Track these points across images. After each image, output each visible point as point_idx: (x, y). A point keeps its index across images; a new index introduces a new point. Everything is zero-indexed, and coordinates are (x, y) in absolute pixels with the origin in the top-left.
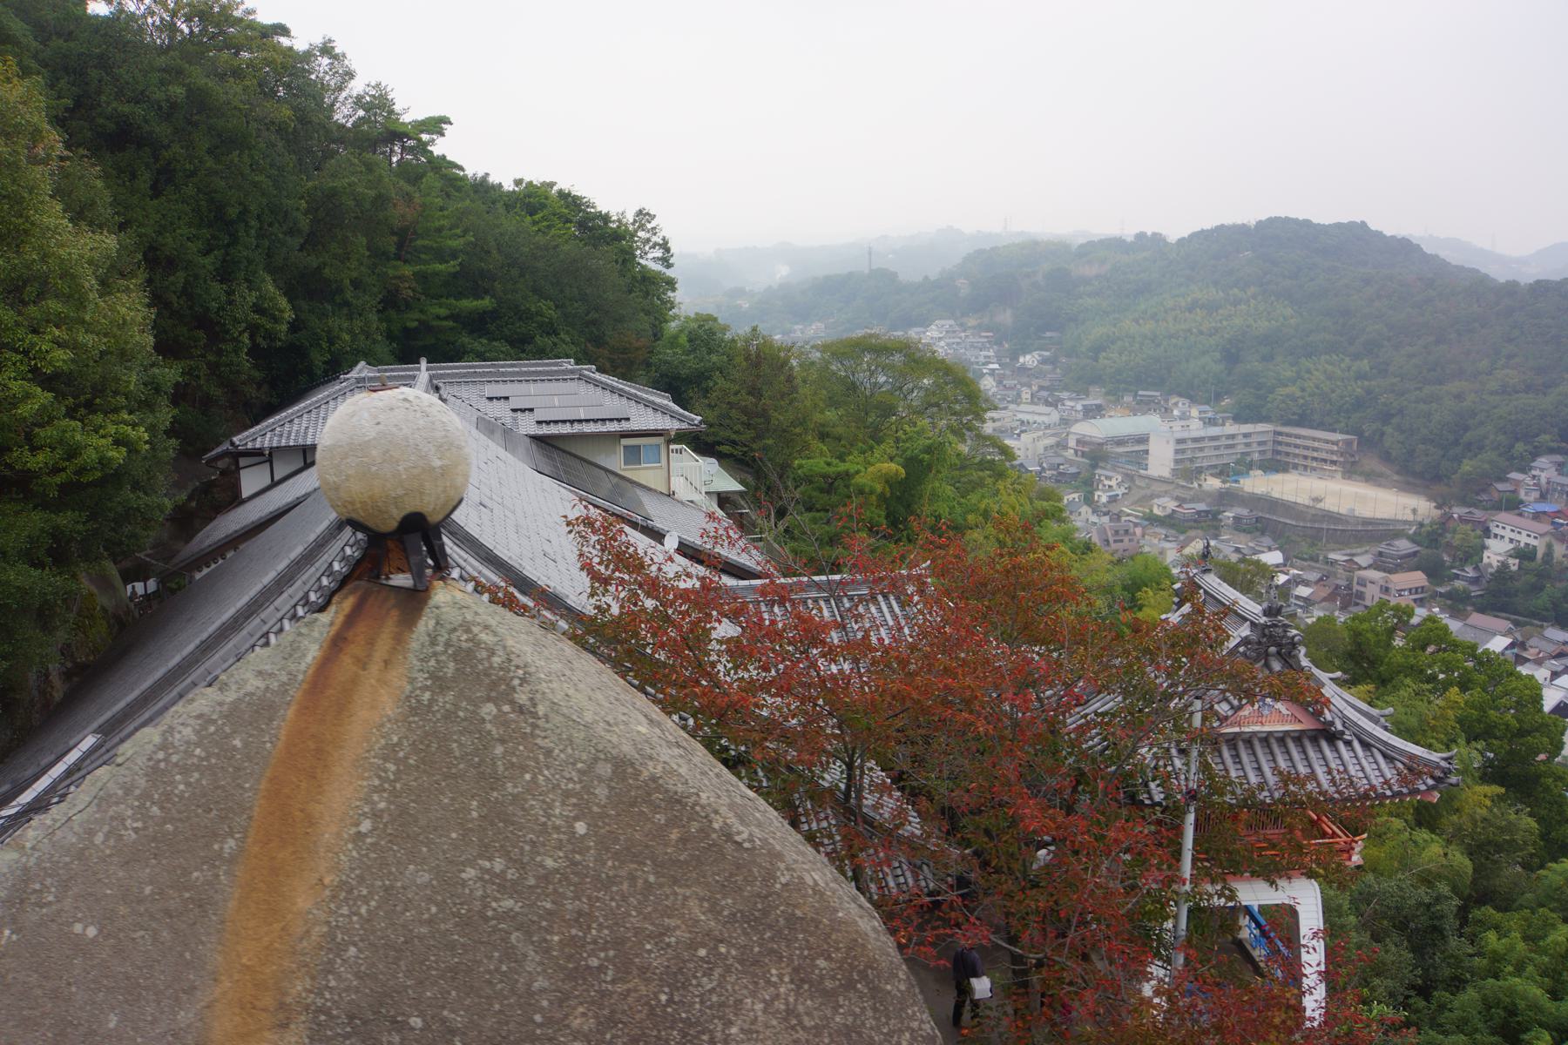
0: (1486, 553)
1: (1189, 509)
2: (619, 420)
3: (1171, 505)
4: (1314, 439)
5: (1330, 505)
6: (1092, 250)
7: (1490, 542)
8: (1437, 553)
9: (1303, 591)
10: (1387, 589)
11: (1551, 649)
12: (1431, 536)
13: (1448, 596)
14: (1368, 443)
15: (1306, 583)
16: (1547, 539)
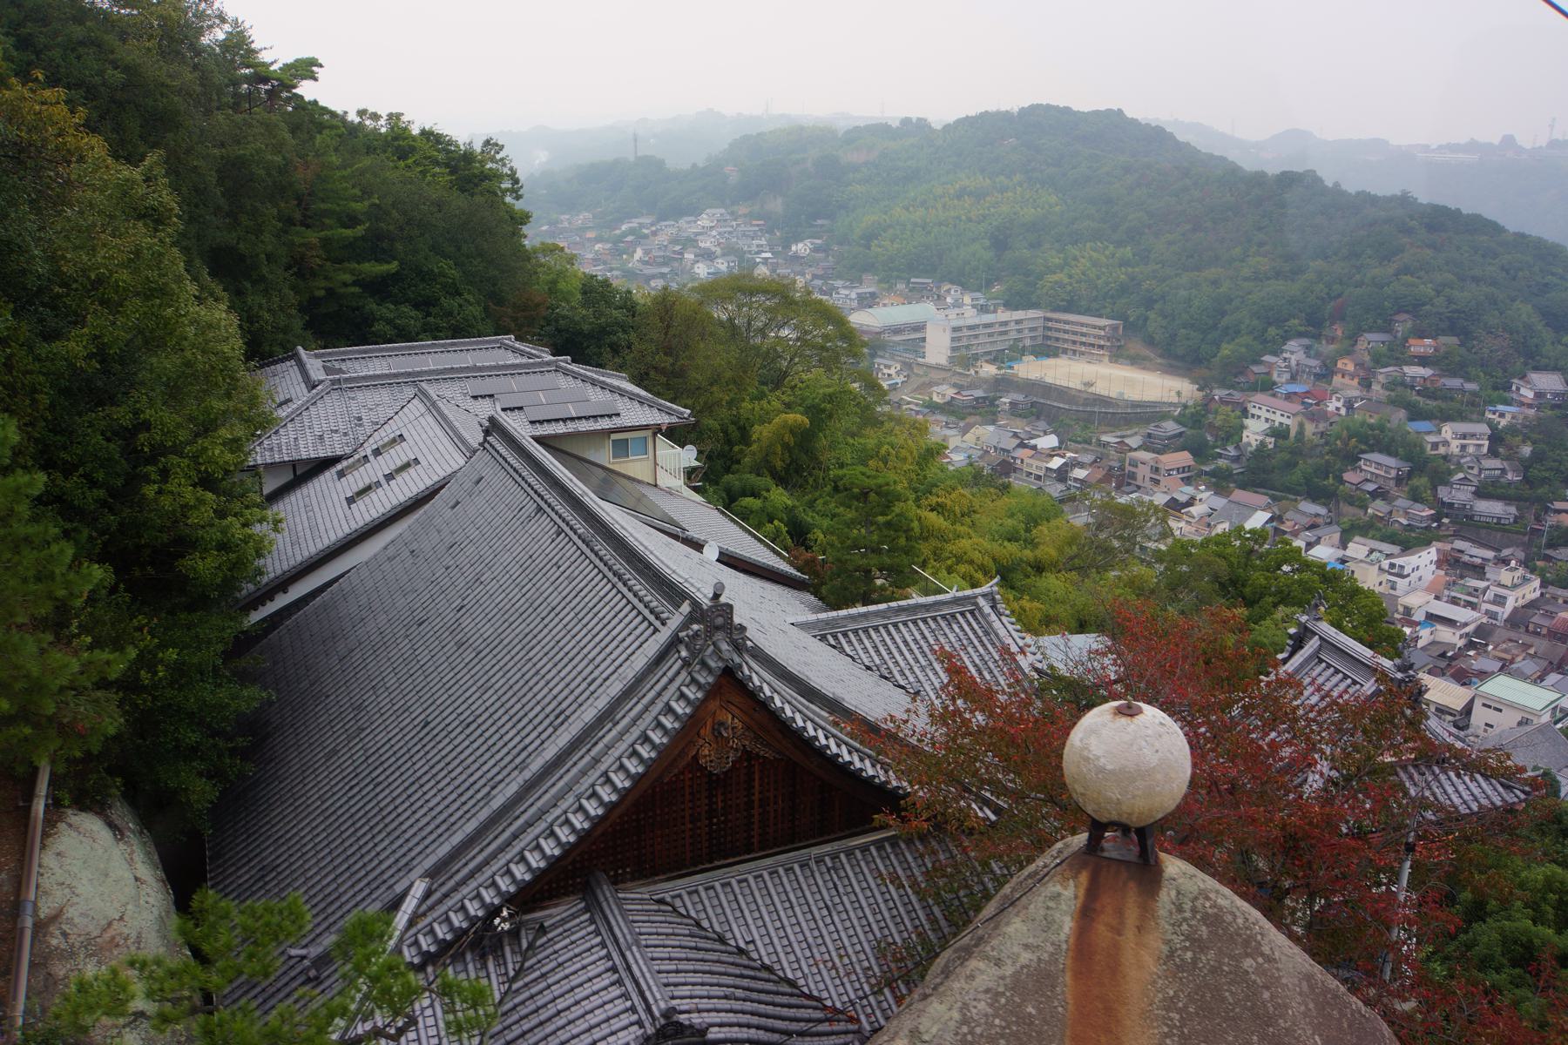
0: (1245, 433)
1: (968, 396)
2: (610, 416)
3: (950, 392)
4: (1082, 325)
5: (1101, 389)
6: (859, 136)
7: (1248, 422)
8: (1203, 439)
9: (1080, 473)
10: (1157, 470)
11: (1305, 521)
12: (1194, 418)
13: (1212, 474)
14: (1133, 327)
15: (1082, 465)
16: (1299, 418)
